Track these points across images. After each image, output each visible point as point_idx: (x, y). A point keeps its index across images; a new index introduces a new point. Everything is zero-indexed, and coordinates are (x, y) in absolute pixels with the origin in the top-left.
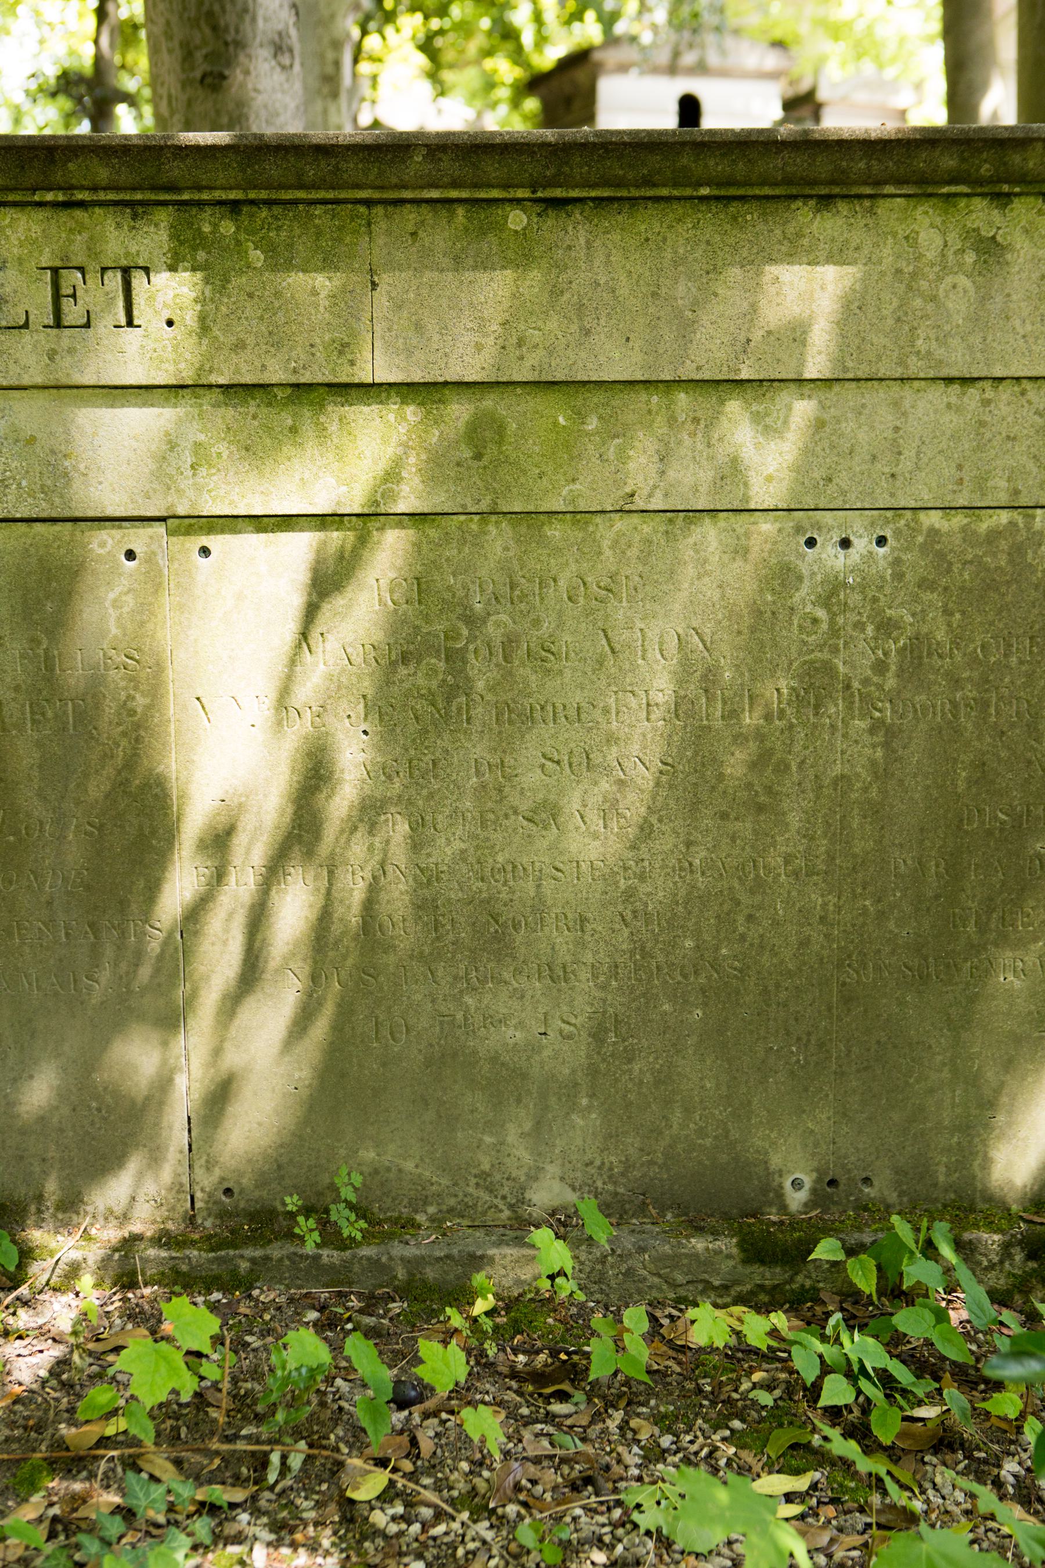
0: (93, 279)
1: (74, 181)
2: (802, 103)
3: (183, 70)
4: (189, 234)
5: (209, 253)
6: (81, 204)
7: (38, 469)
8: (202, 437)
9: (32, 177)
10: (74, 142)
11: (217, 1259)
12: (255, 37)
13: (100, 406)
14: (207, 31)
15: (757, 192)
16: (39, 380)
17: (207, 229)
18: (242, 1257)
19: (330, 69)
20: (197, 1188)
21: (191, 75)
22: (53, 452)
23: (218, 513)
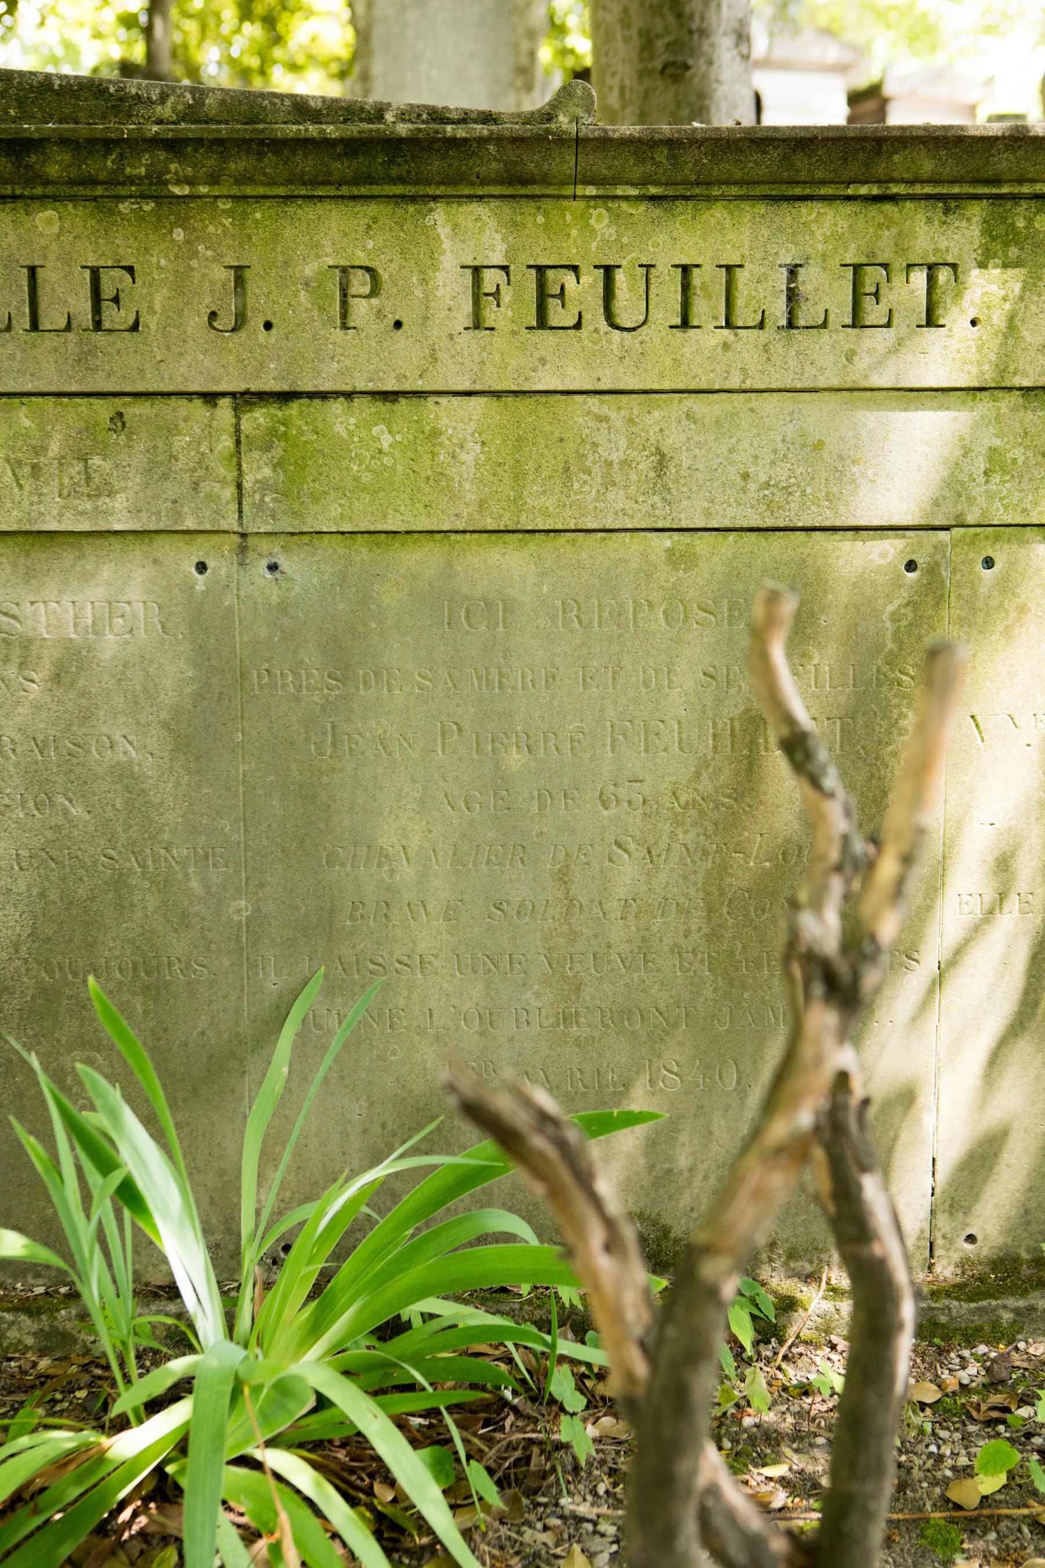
0: (898, 279)
1: (896, 174)
2: (867, 99)
3: (641, 60)
4: (1002, 230)
5: (1022, 249)
6: (893, 198)
7: (824, 475)
8: (997, 442)
9: (854, 169)
10: (908, 133)
11: (978, 1309)
12: (719, 25)
13: (894, 409)
14: (671, 19)
15: (823, 192)
16: (835, 382)
17: (1021, 224)
18: (1005, 1307)
19: (524, 61)
20: (938, 1234)
21: (650, 66)
22: (841, 458)
23: (1010, 521)
